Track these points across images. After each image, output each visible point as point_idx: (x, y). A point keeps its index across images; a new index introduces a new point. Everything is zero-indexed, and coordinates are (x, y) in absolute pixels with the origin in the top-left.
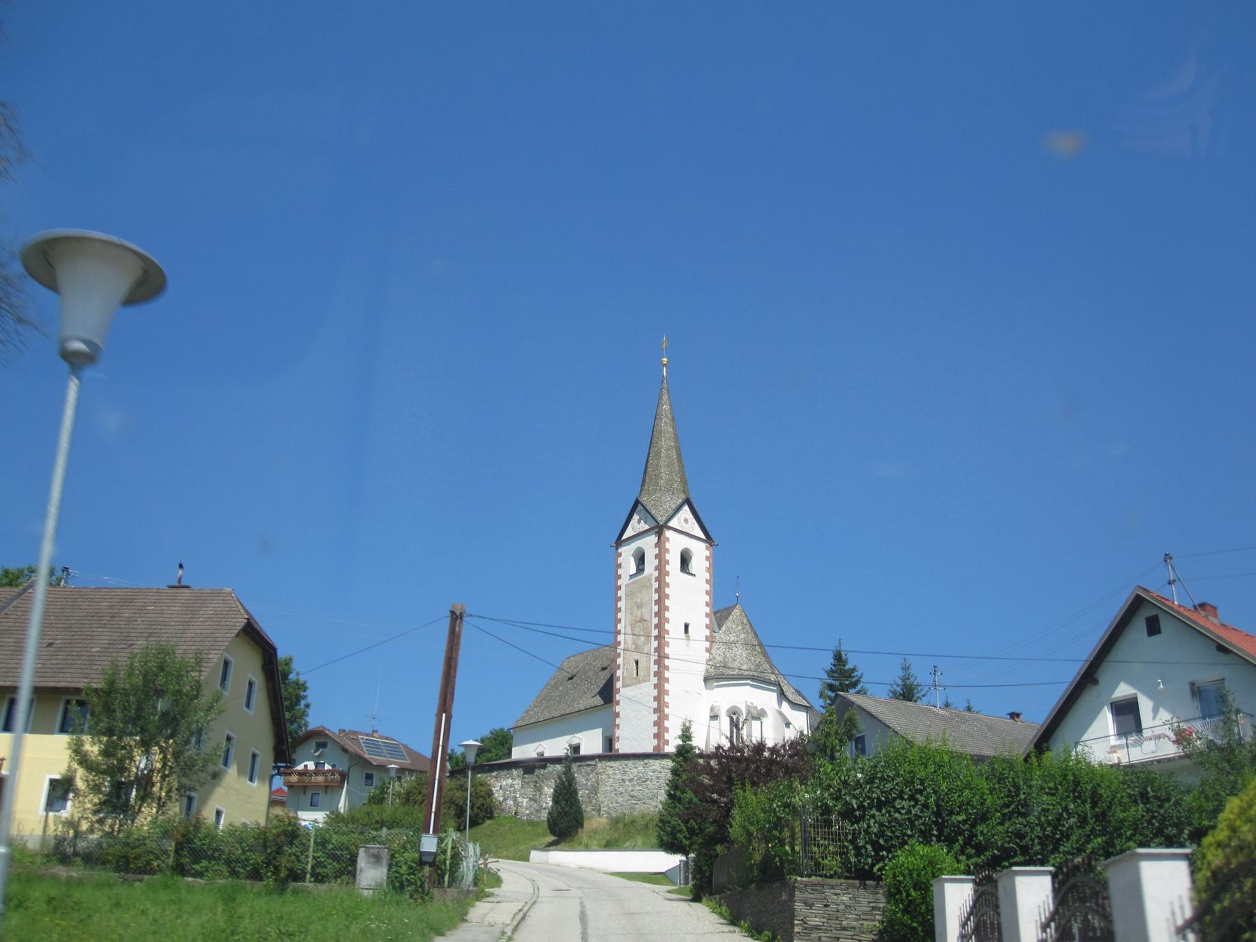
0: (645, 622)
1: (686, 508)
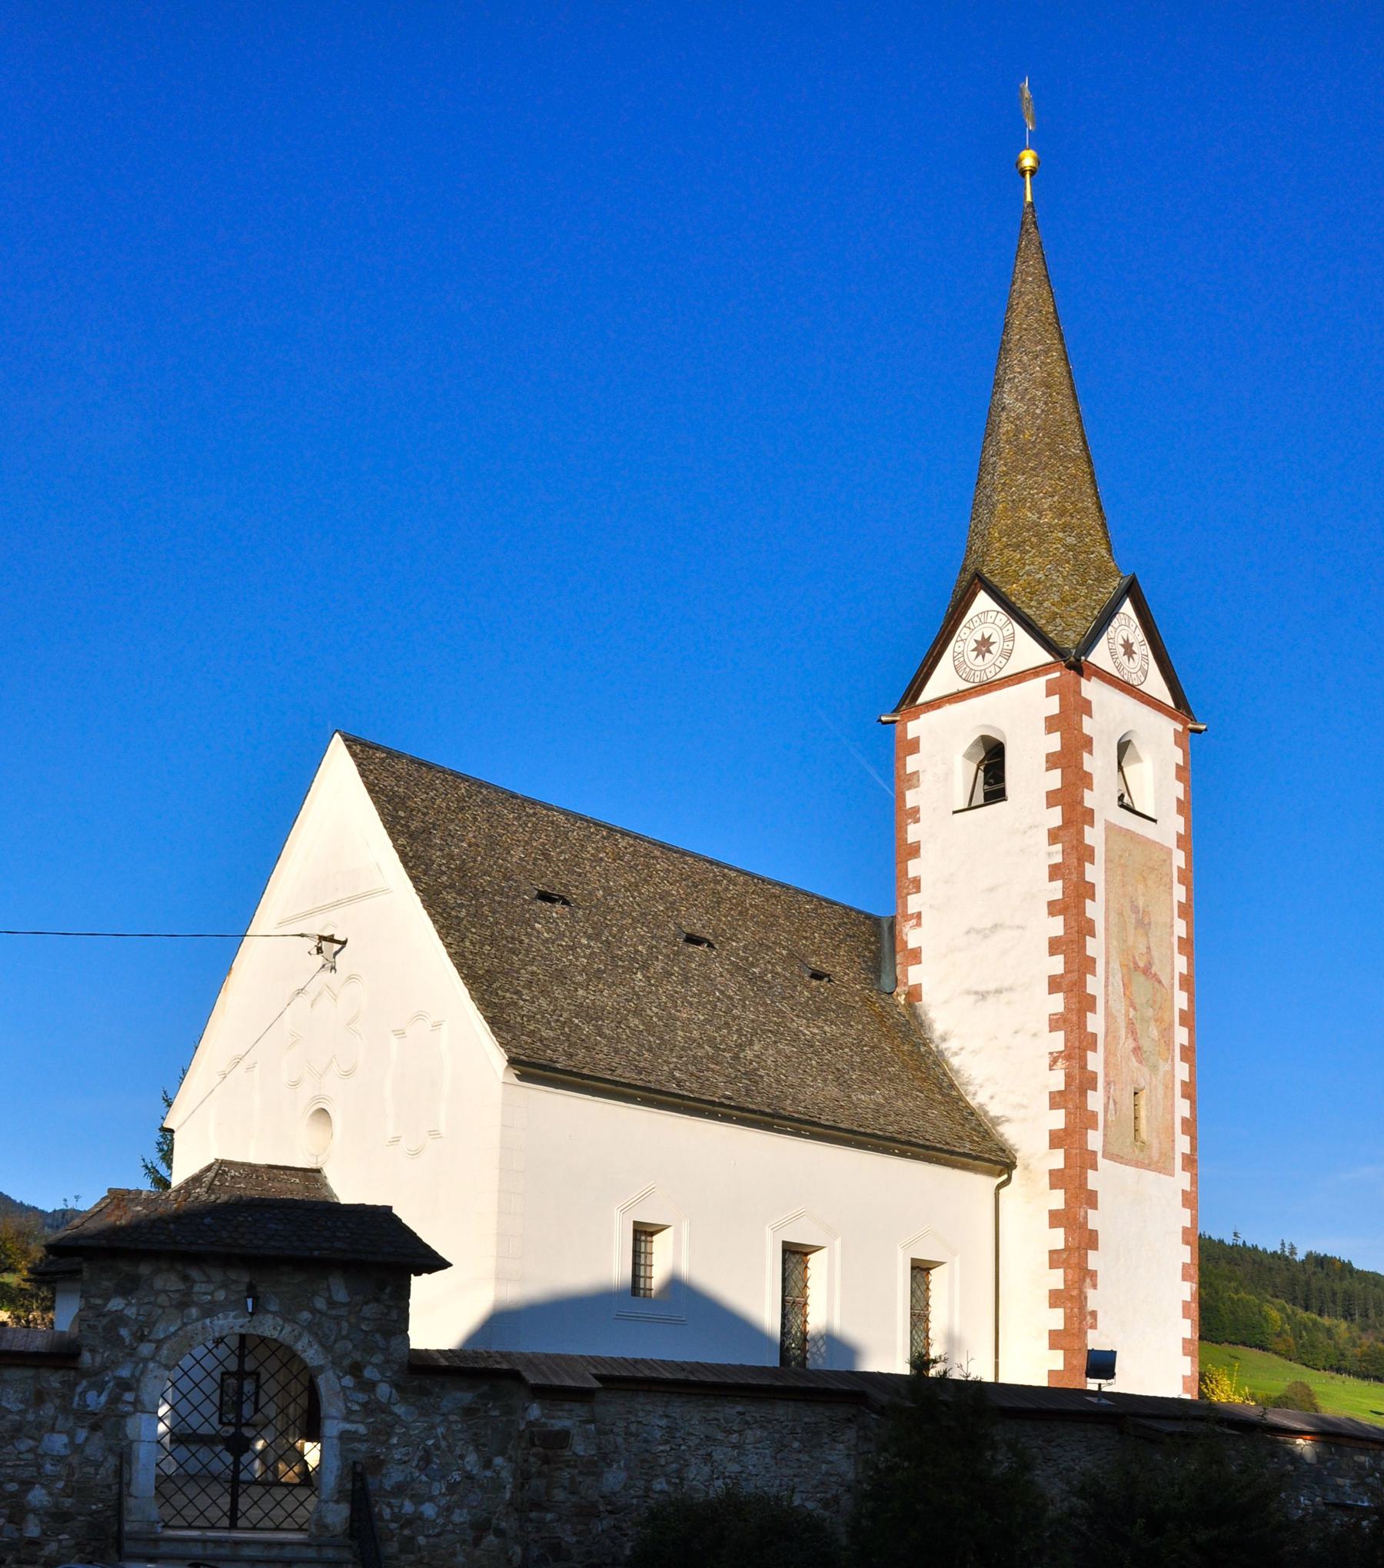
1: (1127, 607)
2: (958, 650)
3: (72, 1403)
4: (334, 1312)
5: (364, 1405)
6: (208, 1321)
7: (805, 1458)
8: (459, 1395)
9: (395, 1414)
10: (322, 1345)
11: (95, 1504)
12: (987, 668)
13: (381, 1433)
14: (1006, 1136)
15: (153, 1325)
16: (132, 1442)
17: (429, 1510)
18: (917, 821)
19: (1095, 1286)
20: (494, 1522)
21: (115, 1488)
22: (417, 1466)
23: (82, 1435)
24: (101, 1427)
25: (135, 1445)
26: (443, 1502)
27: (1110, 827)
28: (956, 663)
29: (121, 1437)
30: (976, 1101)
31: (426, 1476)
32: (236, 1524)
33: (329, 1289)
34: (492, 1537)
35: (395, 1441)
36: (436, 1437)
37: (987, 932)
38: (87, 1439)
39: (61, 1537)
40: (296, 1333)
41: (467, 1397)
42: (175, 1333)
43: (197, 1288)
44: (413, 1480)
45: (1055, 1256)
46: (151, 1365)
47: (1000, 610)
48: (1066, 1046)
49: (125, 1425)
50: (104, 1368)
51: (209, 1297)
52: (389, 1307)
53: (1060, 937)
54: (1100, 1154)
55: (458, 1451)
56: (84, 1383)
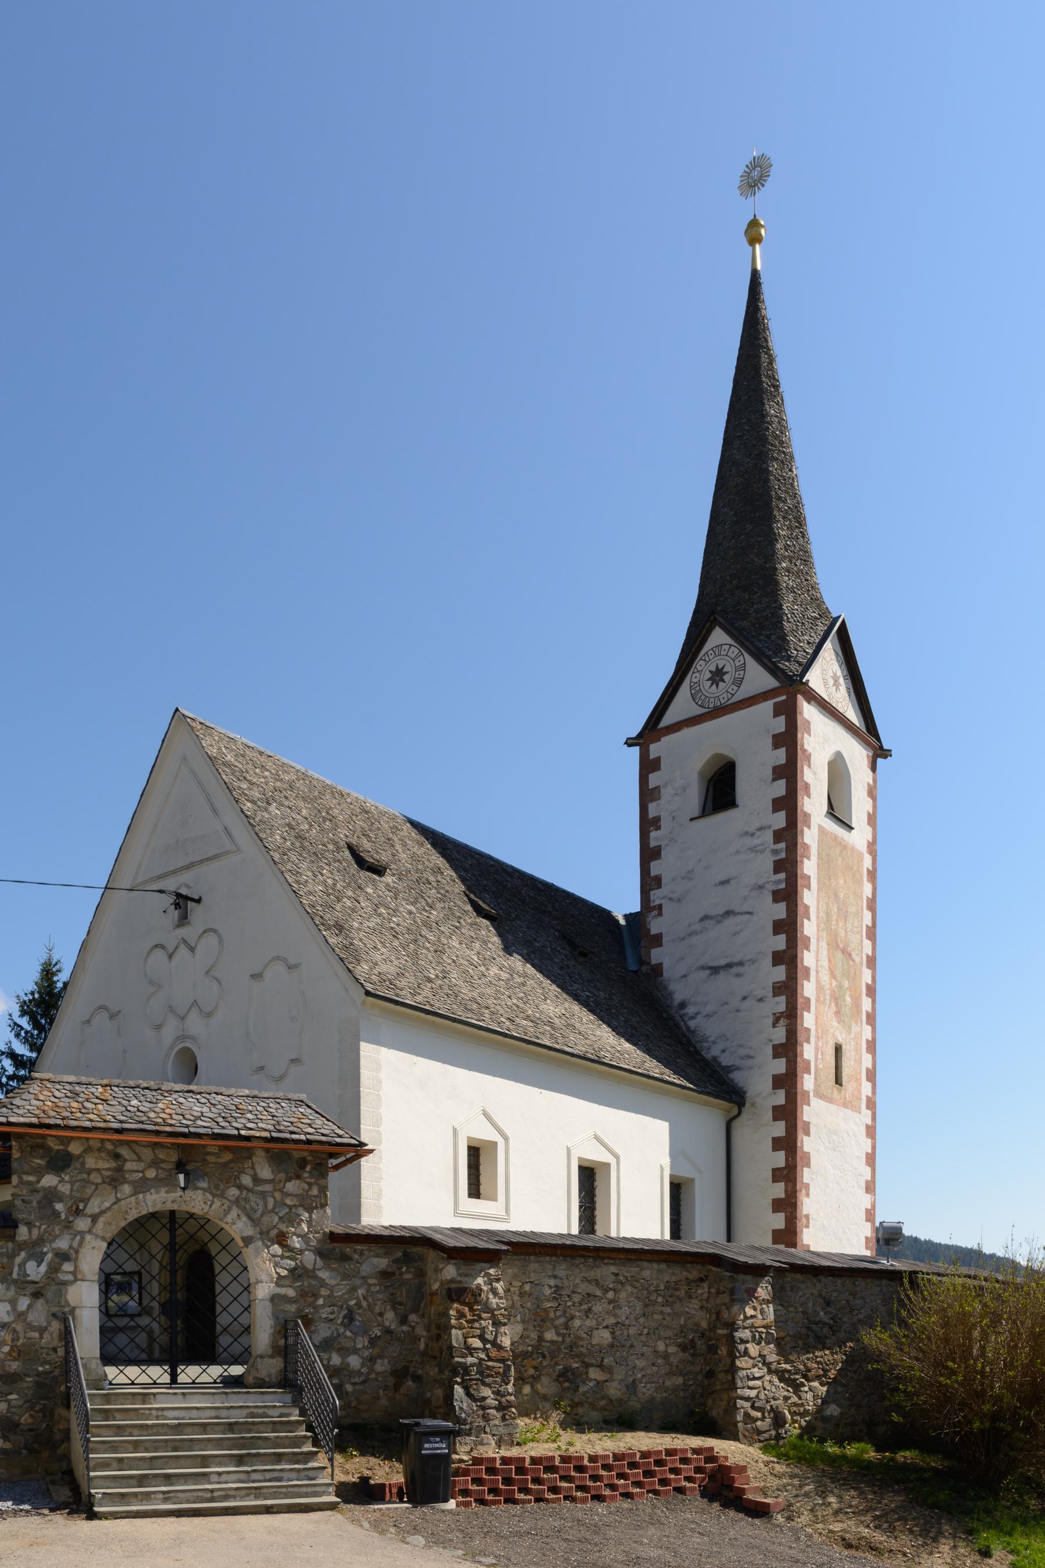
2: (694, 680)
3: (11, 1273)
4: (260, 1188)
5: (292, 1271)
6: (141, 1196)
7: (668, 1310)
8: (376, 1260)
9: (321, 1278)
10: (250, 1218)
11: (42, 1366)
12: (719, 694)
13: (308, 1294)
14: (736, 1081)
15: (86, 1201)
16: (74, 1308)
17: (354, 1361)
18: (658, 828)
19: (808, 1195)
20: (412, 1370)
21: (61, 1352)
22: (342, 1323)
23: (24, 1303)
24: (42, 1295)
25: (77, 1312)
26: (366, 1353)
27: (821, 829)
28: (693, 691)
29: (63, 1304)
30: (709, 1055)
31: (351, 1332)
32: (176, 1379)
33: (253, 1168)
34: (410, 1383)
35: (321, 1301)
36: (357, 1298)
37: (719, 918)
38: (30, 1306)
39: (9, 1397)
40: (225, 1207)
41: (383, 1263)
42: (109, 1208)
43: (128, 1166)
44: (339, 1335)
45: (777, 1173)
46: (88, 1237)
47: (732, 642)
48: (787, 1008)
49: (66, 1292)
50: (41, 1241)
51: (141, 1175)
52: (310, 1185)
53: (783, 920)
54: (811, 1094)
55: (377, 1310)
56: (23, 1254)
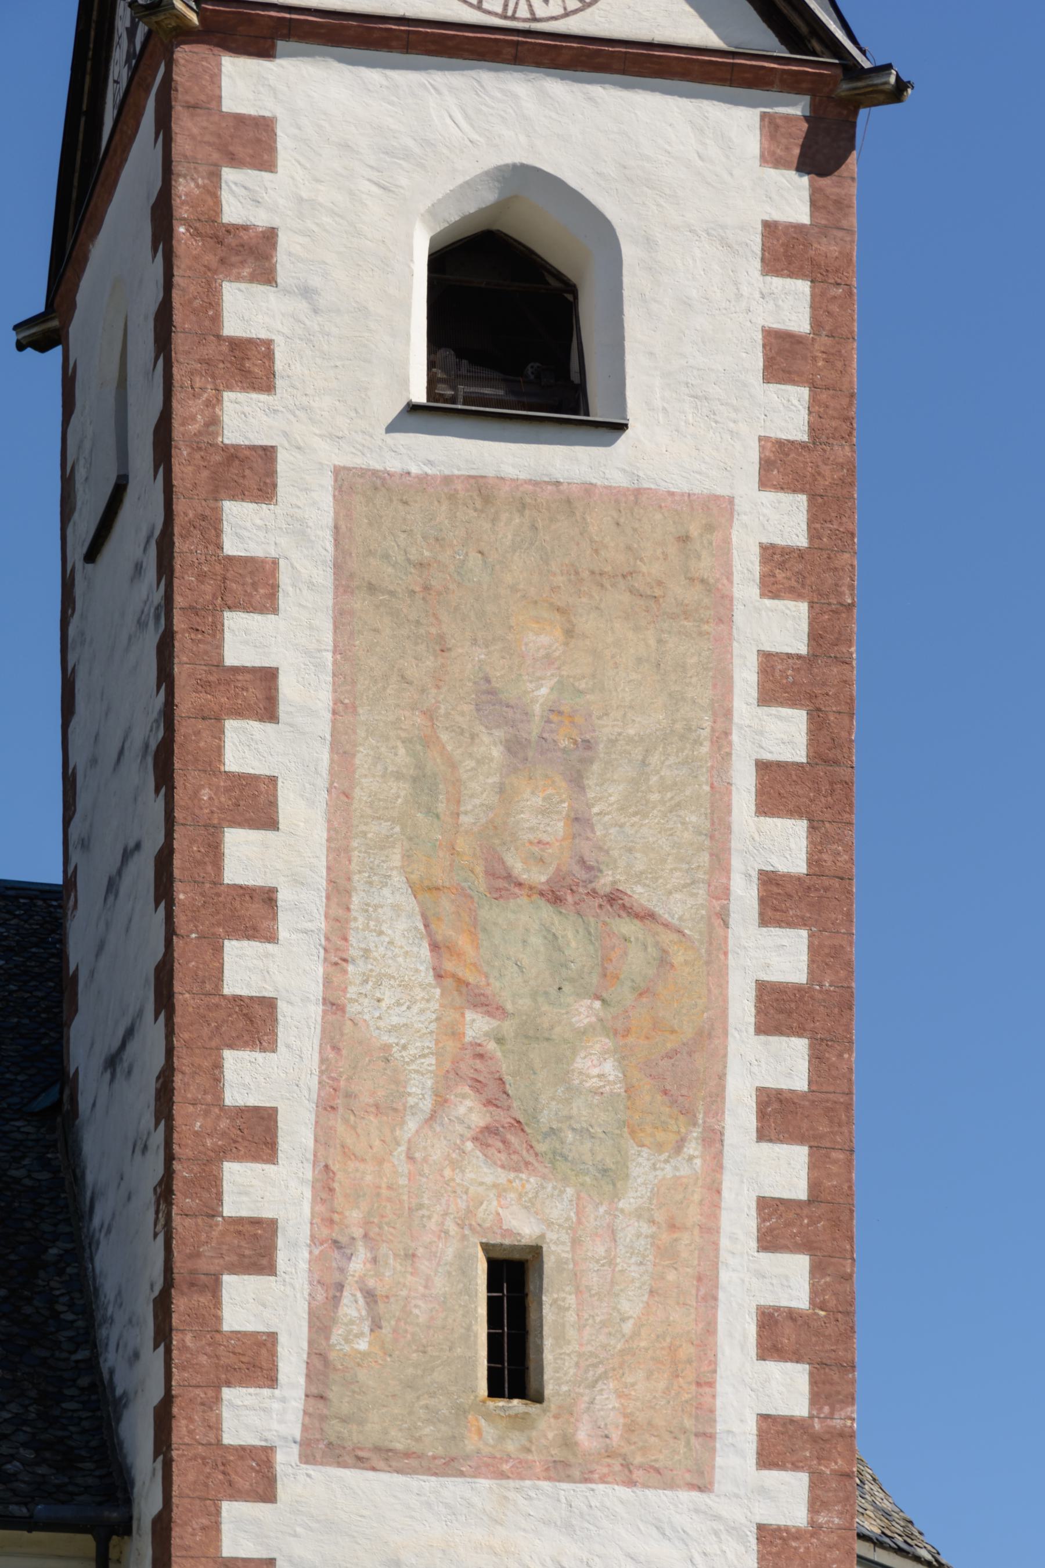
0: (627, 927)
